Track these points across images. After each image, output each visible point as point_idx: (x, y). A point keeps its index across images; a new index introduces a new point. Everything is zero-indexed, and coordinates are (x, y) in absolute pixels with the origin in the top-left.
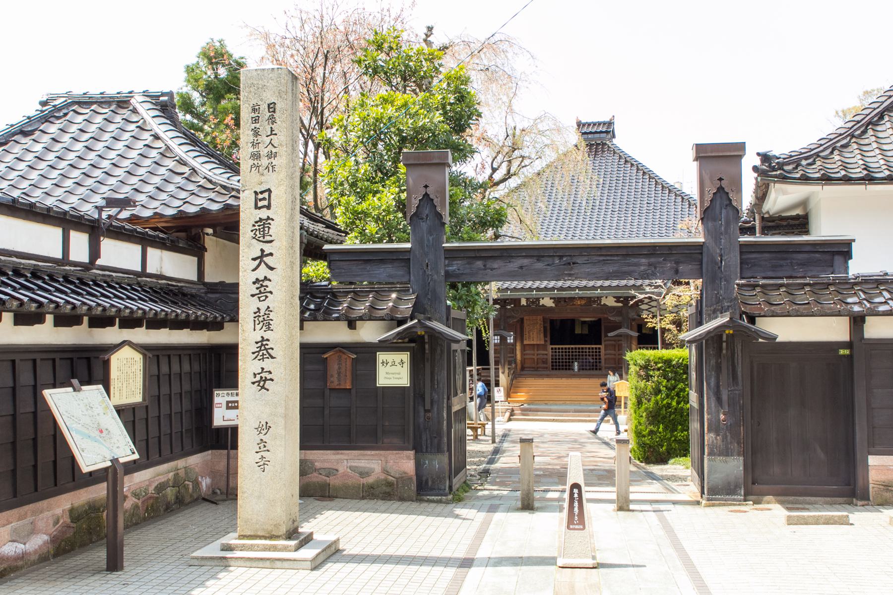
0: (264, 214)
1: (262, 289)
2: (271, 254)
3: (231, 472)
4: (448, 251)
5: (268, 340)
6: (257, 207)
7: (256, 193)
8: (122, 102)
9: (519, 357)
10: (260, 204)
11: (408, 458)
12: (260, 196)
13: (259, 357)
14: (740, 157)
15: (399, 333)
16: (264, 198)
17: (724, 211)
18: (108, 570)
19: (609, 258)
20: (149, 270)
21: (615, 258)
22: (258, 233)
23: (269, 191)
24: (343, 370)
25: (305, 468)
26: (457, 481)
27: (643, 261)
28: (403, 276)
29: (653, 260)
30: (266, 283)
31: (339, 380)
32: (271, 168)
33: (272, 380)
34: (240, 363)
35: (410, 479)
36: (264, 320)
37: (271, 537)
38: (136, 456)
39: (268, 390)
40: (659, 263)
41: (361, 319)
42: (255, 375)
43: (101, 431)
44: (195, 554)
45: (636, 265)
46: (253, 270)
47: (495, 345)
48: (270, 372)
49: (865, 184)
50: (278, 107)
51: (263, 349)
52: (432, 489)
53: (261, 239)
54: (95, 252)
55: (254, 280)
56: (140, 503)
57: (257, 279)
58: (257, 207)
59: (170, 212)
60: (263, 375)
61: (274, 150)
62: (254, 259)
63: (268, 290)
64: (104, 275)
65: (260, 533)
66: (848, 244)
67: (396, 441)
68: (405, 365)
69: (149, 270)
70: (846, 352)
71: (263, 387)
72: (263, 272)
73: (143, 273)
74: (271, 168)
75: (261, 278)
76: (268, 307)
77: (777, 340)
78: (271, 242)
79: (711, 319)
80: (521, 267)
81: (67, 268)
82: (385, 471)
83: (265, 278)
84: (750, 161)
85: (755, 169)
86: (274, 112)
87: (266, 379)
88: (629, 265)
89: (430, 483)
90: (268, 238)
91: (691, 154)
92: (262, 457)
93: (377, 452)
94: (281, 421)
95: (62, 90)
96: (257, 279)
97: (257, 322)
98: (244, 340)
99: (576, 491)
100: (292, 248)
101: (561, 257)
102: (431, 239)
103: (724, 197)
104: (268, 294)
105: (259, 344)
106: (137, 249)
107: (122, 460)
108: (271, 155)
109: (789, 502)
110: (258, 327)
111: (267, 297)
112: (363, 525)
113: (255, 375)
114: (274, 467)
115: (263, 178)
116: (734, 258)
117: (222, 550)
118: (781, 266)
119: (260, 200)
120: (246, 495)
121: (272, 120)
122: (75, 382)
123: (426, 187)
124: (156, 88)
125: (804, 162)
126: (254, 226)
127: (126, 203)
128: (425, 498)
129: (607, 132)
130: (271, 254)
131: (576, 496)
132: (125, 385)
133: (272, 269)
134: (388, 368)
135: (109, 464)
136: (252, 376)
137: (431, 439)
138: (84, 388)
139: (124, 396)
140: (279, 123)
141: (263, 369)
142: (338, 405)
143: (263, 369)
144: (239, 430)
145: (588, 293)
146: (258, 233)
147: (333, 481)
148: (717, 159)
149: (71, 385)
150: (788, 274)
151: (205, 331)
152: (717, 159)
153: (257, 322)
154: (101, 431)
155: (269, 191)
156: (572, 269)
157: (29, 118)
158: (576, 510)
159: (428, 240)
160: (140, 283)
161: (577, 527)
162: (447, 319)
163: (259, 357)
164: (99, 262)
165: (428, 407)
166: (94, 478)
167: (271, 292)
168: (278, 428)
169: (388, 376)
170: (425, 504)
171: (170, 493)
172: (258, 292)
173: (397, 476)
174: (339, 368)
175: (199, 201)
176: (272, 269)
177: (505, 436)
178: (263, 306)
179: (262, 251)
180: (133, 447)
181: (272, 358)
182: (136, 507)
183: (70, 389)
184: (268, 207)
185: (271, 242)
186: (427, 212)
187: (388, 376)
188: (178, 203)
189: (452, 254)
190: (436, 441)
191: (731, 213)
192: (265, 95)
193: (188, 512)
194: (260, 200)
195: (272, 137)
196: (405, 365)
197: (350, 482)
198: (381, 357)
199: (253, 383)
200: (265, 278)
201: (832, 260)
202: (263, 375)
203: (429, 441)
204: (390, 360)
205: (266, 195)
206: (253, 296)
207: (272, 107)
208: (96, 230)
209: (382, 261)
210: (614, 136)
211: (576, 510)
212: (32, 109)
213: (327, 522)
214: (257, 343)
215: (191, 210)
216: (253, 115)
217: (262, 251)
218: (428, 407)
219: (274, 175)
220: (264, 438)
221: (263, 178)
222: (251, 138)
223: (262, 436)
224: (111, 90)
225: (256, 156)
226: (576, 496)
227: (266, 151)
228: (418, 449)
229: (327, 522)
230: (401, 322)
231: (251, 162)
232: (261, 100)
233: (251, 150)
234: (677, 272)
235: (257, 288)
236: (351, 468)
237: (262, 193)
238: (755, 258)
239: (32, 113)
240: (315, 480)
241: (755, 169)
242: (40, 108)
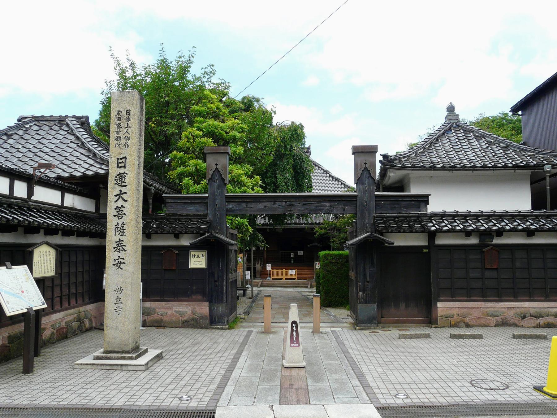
0: (122, 170)
1: (120, 212)
2: (125, 193)
3: (101, 315)
4: (227, 197)
5: (123, 241)
6: (118, 167)
7: (118, 159)
8: (61, 121)
9: (265, 256)
10: (120, 165)
11: (205, 306)
12: (120, 161)
14: (376, 152)
15: (201, 240)
16: (122, 162)
17: (367, 180)
18: (23, 373)
20: (66, 204)
23: (125, 158)
25: (145, 312)
26: (231, 318)
27: (328, 204)
28: (204, 211)
29: (333, 204)
30: (122, 209)
34: (107, 254)
35: (206, 317)
36: (121, 230)
37: (122, 352)
38: (45, 306)
39: (122, 269)
40: (335, 205)
41: (181, 233)
43: (23, 292)
44: (79, 362)
45: (323, 206)
46: (116, 202)
47: (254, 251)
48: (123, 259)
49: (432, 170)
50: (132, 112)
51: (120, 246)
52: (218, 322)
54: (30, 193)
56: (55, 332)
58: (118, 167)
59: (79, 174)
60: (119, 260)
61: (129, 136)
62: (116, 196)
63: (123, 213)
64: (35, 205)
65: (116, 350)
66: (427, 196)
67: (200, 297)
68: (204, 257)
69: (66, 204)
70: (427, 251)
71: (119, 267)
72: (120, 203)
73: (62, 206)
78: (126, 186)
79: (361, 235)
80: (265, 207)
81: (12, 200)
82: (193, 313)
83: (122, 206)
84: (378, 157)
85: (380, 161)
86: (129, 115)
87: (121, 263)
89: (217, 319)
90: (124, 184)
91: (350, 151)
94: (129, 286)
95: (30, 114)
98: (109, 241)
99: (294, 325)
100: (138, 190)
101: (286, 202)
103: (367, 172)
104: (123, 215)
106: (59, 194)
107: (34, 309)
108: (127, 138)
109: (399, 327)
110: (117, 233)
111: (122, 217)
112: (179, 343)
115: (122, 151)
116: (373, 203)
117: (94, 359)
119: (120, 163)
121: (128, 119)
122: (8, 263)
123: (217, 165)
124: (79, 114)
125: (403, 160)
127: (49, 166)
128: (214, 327)
129: (307, 152)
130: (125, 193)
131: (294, 328)
132: (43, 266)
133: (126, 201)
134: (196, 259)
135: (26, 311)
136: (113, 261)
138: (13, 267)
139: (43, 272)
141: (119, 257)
142: (162, 277)
143: (119, 257)
144: (106, 291)
145: (299, 226)
147: (165, 319)
148: (363, 153)
149: (5, 265)
150: (398, 211)
151: (98, 238)
152: (363, 153)
154: (23, 292)
155: (125, 158)
156: (291, 208)
157: (10, 127)
158: (295, 335)
159: (217, 192)
160: (59, 211)
161: (295, 345)
162: (227, 234)
164: (33, 198)
165: (216, 279)
166: (15, 319)
167: (125, 214)
168: (128, 290)
170: (214, 330)
171: (75, 325)
175: (95, 169)
176: (126, 201)
177: (258, 294)
178: (120, 222)
179: (121, 191)
180: (43, 300)
182: (53, 333)
183: (5, 267)
184: (125, 167)
185: (126, 186)
186: (217, 178)
188: (83, 170)
189: (230, 199)
191: (371, 180)
193: (84, 335)
194: (120, 163)
196: (204, 257)
197: (174, 319)
198: (192, 253)
199: (114, 265)
200: (122, 206)
201: (420, 205)
202: (119, 260)
204: (196, 255)
205: (123, 160)
206: (115, 216)
207: (128, 112)
208: (31, 181)
209: (194, 203)
210: (310, 154)
211: (295, 335)
212: (13, 122)
213: (159, 341)
214: (116, 242)
215: (90, 173)
217: (121, 191)
218: (216, 279)
219: (128, 149)
220: (119, 296)
224: (56, 114)
225: (118, 139)
226: (294, 328)
227: (124, 136)
228: (211, 302)
229: (159, 341)
230: (202, 235)
231: (116, 142)
233: (116, 135)
234: (344, 210)
236: (175, 311)
237: (121, 159)
239: (12, 124)
241: (380, 161)
242: (17, 122)
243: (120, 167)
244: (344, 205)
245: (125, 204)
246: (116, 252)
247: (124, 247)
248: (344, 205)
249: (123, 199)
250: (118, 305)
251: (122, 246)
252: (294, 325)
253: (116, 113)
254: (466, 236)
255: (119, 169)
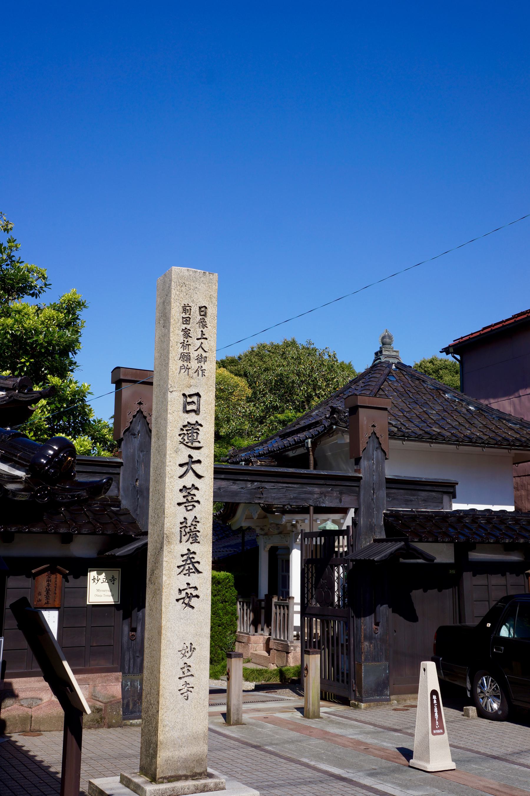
0: (192, 418)
1: (190, 498)
2: (199, 462)
5: (194, 553)
7: (184, 395)
10: (189, 408)
11: (117, 679)
12: (189, 400)
13: (185, 572)
17: (375, 453)
19: (290, 485)
21: (295, 486)
22: (186, 438)
23: (198, 395)
24: (52, 588)
27: (316, 490)
29: (324, 489)
30: (194, 492)
31: (47, 597)
32: (200, 372)
33: (197, 596)
40: (328, 492)
42: (180, 591)
46: (181, 477)
50: (209, 311)
53: (189, 444)
55: (181, 488)
57: (184, 487)
60: (189, 591)
61: (204, 355)
62: (181, 465)
63: (195, 499)
65: (181, 773)
66: (453, 485)
72: (190, 480)
74: (200, 372)
75: (189, 486)
76: (195, 517)
77: (435, 561)
78: (199, 448)
83: (193, 485)
86: (205, 315)
88: (306, 493)
90: (196, 444)
92: (187, 683)
93: (85, 676)
96: (184, 487)
97: (184, 533)
99: (434, 697)
102: (141, 455)
103: (376, 440)
104: (196, 504)
105: (185, 557)
110: (184, 539)
113: (180, 591)
114: (198, 693)
115: (192, 382)
118: (411, 501)
119: (189, 403)
120: (167, 729)
121: (203, 324)
126: (182, 430)
130: (199, 462)
131: (435, 702)
133: (199, 477)
137: (134, 658)
140: (209, 327)
146: (186, 438)
153: (184, 533)
155: (198, 395)
158: (436, 715)
159: (139, 456)
161: (438, 731)
163: (185, 572)
167: (198, 502)
169: (99, 593)
172: (184, 500)
173: (105, 701)
174: (48, 585)
176: (199, 477)
178: (190, 517)
179: (190, 457)
181: (199, 572)
184: (196, 412)
185: (199, 448)
187: (99, 593)
190: (139, 660)
192: (196, 296)
194: (189, 403)
195: (202, 340)
196: (116, 582)
199: (178, 600)
203: (132, 661)
205: (195, 399)
206: (179, 504)
207: (203, 310)
211: (436, 715)
214: (182, 556)
216: (184, 315)
217: (190, 457)
219: (204, 379)
221: (192, 381)
222: (182, 339)
223: (185, 660)
226: (435, 702)
227: (196, 353)
231: (181, 363)
232: (193, 301)
233: (181, 350)
235: (184, 497)
237: (190, 396)
238: (394, 493)
240: (15, 713)
243: (188, 412)
244: (341, 493)
245: (198, 483)
246: (182, 575)
247: (196, 565)
248: (341, 493)
249: (194, 472)
250: (186, 679)
251: (193, 563)
252: (434, 697)
253: (181, 310)
254: (505, 551)
255: (186, 415)
